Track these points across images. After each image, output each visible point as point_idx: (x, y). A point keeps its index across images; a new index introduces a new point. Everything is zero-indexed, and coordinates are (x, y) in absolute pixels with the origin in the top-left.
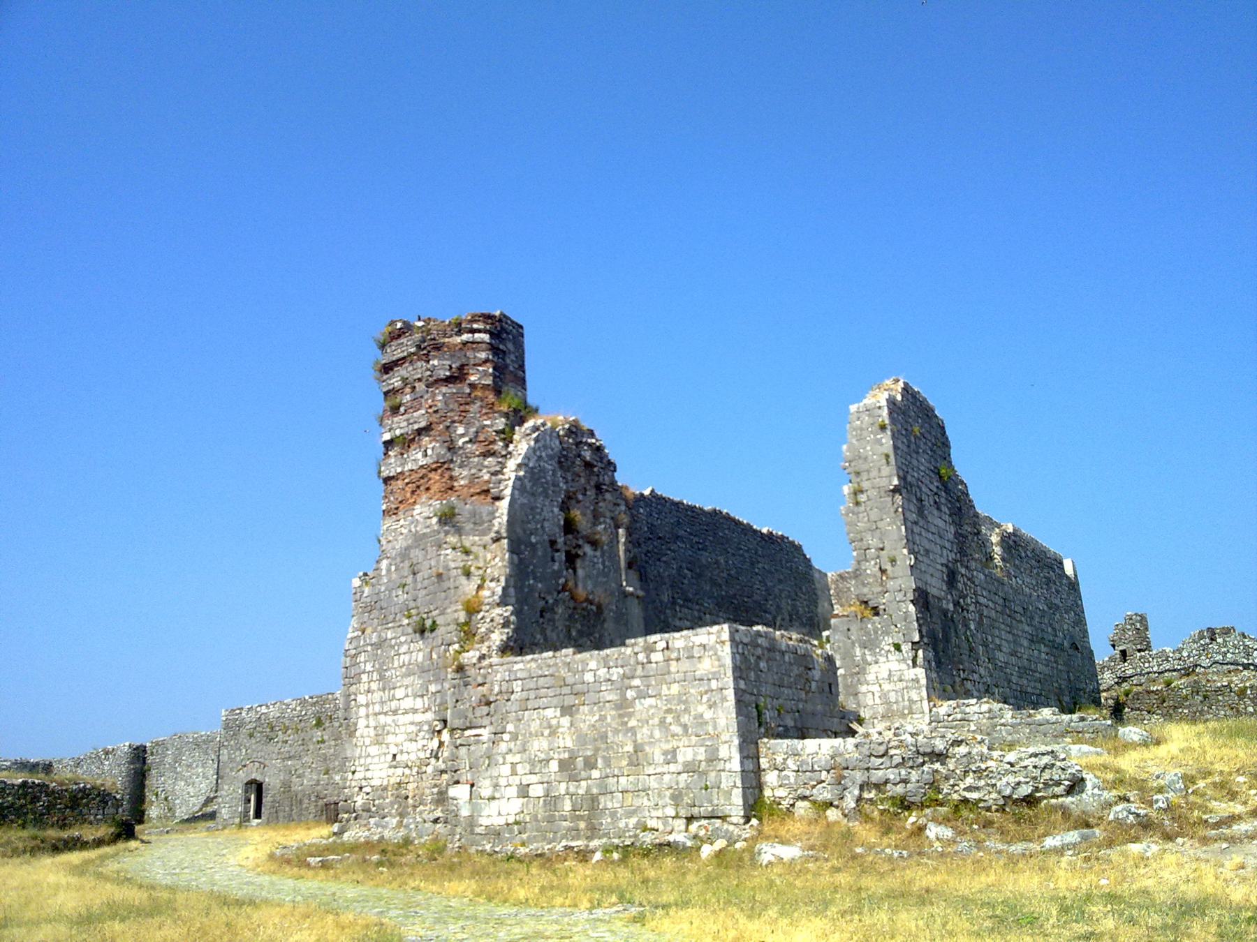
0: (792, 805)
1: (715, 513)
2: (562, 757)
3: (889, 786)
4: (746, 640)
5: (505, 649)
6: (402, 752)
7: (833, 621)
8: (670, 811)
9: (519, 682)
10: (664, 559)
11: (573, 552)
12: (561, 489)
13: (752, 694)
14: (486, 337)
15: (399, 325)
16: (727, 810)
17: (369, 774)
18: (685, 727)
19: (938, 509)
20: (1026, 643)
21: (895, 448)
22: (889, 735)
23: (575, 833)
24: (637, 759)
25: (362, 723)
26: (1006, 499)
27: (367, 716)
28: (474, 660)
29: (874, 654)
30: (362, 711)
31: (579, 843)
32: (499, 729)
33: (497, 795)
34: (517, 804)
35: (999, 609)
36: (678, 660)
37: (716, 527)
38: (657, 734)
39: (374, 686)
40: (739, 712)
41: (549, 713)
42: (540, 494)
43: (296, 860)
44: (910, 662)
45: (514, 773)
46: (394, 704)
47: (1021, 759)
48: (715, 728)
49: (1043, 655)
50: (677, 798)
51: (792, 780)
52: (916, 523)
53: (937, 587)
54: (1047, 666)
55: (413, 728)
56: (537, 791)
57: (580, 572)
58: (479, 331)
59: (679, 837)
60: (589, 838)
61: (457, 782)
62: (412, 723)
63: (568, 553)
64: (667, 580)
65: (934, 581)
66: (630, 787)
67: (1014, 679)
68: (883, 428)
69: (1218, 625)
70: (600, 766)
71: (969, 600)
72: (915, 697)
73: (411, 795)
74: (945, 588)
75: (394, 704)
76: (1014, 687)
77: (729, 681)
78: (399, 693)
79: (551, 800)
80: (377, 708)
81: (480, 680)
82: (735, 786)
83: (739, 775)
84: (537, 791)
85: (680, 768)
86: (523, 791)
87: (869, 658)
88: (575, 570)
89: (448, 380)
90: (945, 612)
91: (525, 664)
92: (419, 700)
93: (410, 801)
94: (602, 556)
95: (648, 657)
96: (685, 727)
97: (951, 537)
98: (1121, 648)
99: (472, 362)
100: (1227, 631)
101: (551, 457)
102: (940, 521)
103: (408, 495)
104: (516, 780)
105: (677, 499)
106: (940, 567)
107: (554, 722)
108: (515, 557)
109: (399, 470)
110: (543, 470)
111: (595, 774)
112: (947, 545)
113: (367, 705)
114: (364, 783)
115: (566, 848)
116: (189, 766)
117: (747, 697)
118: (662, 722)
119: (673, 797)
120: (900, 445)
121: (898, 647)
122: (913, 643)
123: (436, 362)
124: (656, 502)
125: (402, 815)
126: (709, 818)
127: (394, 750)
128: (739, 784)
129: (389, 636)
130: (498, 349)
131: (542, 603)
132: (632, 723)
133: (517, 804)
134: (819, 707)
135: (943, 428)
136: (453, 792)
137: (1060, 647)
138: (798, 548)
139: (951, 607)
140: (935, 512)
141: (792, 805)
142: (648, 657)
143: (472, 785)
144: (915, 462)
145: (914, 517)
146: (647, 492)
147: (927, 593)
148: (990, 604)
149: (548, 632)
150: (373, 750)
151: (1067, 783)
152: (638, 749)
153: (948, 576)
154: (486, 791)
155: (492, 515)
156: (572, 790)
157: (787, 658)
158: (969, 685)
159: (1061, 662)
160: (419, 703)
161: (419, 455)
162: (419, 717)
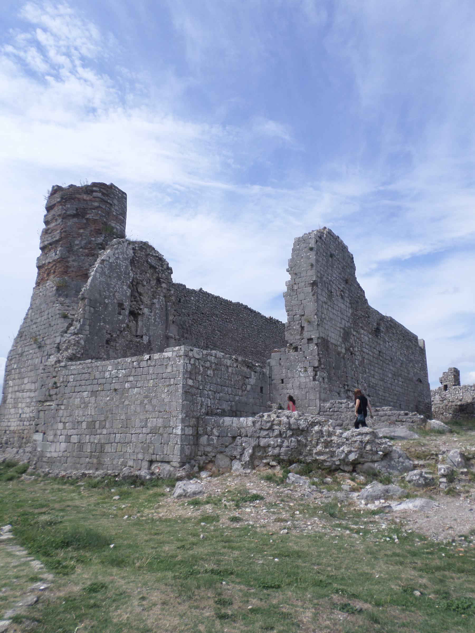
0: (215, 456)
1: (238, 305)
3: (270, 449)
9: (73, 376)
10: (204, 324)
11: (136, 311)
12: (130, 277)
13: (198, 388)
14: (99, 195)
17: (9, 424)
18: (154, 406)
20: (390, 375)
21: (317, 261)
24: (126, 426)
32: (60, 403)
33: (55, 441)
34: (63, 445)
35: (375, 356)
36: (155, 366)
41: (85, 394)
42: (115, 277)
44: (311, 378)
45: (64, 428)
48: (170, 408)
49: (400, 383)
50: (145, 450)
51: (215, 441)
53: (334, 337)
54: (402, 388)
55: (28, 400)
56: (75, 439)
57: (140, 323)
58: (96, 191)
59: (144, 473)
60: (97, 469)
64: (204, 335)
66: (122, 441)
67: (381, 393)
68: (311, 249)
70: (107, 427)
71: (356, 349)
72: (312, 397)
73: (25, 437)
74: (341, 340)
76: (380, 397)
78: (26, 381)
79: (81, 445)
81: (54, 374)
82: (177, 444)
83: (179, 437)
84: (75, 439)
86: (68, 437)
87: (289, 375)
88: (137, 322)
89: (74, 216)
90: (339, 353)
92: (33, 384)
93: (24, 440)
94: (155, 315)
95: (139, 364)
96: (154, 406)
97: (349, 315)
98: (445, 384)
99: (90, 207)
103: (45, 276)
104: (65, 432)
105: (216, 294)
106: (338, 329)
107: (87, 400)
108: (92, 309)
109: (44, 262)
111: (105, 431)
118: (142, 403)
119: (143, 448)
120: (321, 259)
122: (314, 367)
123: (69, 206)
126: (162, 462)
127: (20, 411)
128: (179, 443)
131: (109, 336)
133: (63, 445)
134: (251, 400)
135: (352, 258)
137: (411, 380)
139: (343, 351)
140: (340, 300)
141: (215, 456)
142: (139, 364)
143: (44, 433)
144: (330, 272)
147: (328, 341)
148: (370, 353)
150: (12, 411)
151: (381, 453)
152: (128, 419)
153: (344, 334)
154: (51, 438)
156: (92, 440)
157: (230, 370)
159: (410, 387)
160: (33, 387)
162: (32, 394)
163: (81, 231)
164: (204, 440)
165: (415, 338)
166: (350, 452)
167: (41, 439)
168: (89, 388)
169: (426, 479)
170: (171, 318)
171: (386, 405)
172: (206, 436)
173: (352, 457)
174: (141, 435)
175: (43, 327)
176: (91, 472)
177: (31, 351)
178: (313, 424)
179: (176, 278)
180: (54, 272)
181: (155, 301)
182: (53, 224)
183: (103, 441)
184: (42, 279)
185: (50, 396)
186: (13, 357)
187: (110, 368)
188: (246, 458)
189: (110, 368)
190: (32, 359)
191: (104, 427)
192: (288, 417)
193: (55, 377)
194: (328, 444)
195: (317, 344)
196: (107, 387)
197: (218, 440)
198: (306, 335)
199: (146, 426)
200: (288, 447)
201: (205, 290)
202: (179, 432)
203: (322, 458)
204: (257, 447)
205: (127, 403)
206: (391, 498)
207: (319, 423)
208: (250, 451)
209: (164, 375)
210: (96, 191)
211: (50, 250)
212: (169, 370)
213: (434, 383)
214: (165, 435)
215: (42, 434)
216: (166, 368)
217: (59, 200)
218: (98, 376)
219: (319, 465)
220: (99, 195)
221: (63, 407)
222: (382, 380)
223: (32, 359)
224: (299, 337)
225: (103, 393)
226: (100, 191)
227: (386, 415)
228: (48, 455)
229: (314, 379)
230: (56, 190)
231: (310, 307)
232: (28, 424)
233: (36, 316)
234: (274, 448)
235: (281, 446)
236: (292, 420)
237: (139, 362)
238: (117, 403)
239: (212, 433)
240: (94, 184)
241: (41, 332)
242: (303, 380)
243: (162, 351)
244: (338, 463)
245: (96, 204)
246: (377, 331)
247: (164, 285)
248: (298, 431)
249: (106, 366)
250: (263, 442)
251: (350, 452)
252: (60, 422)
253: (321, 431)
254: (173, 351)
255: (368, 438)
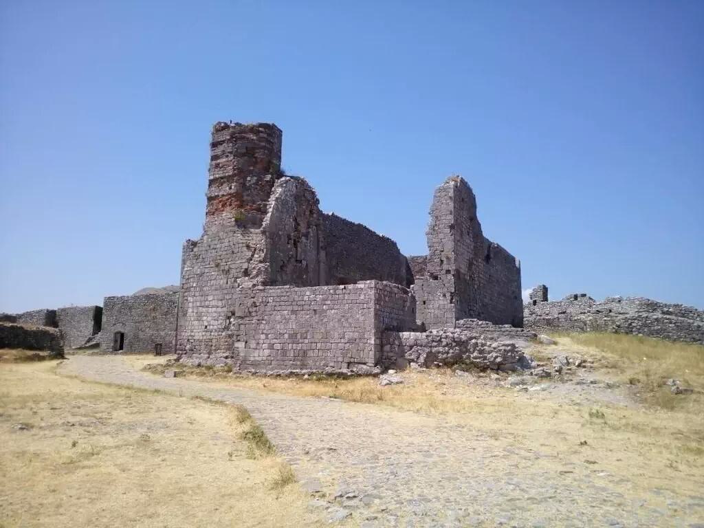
1: (359, 225)
2: (290, 332)
4: (381, 288)
5: (264, 284)
6: (210, 325)
7: (416, 281)
8: (340, 359)
14: (265, 136)
15: (222, 125)
16: (367, 360)
17: (192, 334)
18: (350, 324)
19: (468, 235)
20: (496, 295)
22: (441, 333)
23: (295, 366)
24: (326, 336)
25: (190, 310)
26: (492, 231)
27: (193, 307)
28: (250, 286)
29: (432, 295)
30: (191, 305)
31: (297, 371)
32: (261, 318)
34: (267, 352)
36: (349, 294)
37: (360, 232)
38: (337, 325)
39: (197, 294)
40: (375, 319)
41: (286, 312)
43: (151, 369)
44: (449, 301)
45: (267, 338)
46: (207, 303)
47: (499, 346)
52: (458, 241)
53: (464, 270)
56: (278, 346)
61: (239, 341)
62: (215, 312)
63: (295, 240)
65: (463, 266)
69: (579, 293)
73: (214, 345)
75: (207, 303)
77: (372, 304)
78: (210, 298)
79: (284, 352)
80: (198, 304)
81: (252, 295)
84: (278, 346)
85: (346, 341)
91: (274, 291)
92: (220, 302)
93: (213, 348)
95: (335, 292)
96: (350, 324)
100: (584, 295)
101: (291, 196)
102: (468, 240)
105: (344, 217)
109: (216, 194)
110: (287, 201)
111: (306, 341)
112: (470, 250)
113: (193, 302)
114: (190, 338)
115: (291, 372)
116: (78, 322)
117: (379, 313)
118: (339, 320)
121: (444, 296)
124: (334, 218)
125: (210, 353)
127: (206, 324)
128: (373, 349)
129: (206, 271)
130: (270, 141)
132: (325, 320)
133: (267, 352)
136: (237, 345)
138: (394, 244)
142: (335, 292)
143: (246, 342)
145: (458, 238)
146: (330, 214)
149: (283, 276)
150: (196, 323)
152: (327, 332)
155: (262, 220)
158: (472, 312)
160: (220, 304)
161: (227, 188)
162: (219, 310)
163: (252, 168)
164: (387, 348)
165: (513, 259)
166: (497, 357)
167: (244, 347)
168: (290, 308)
169: (546, 372)
170: (321, 244)
171: (507, 324)
172: (389, 346)
173: (499, 360)
174: (340, 344)
175: (225, 253)
176: (297, 371)
177: (213, 273)
178: (471, 338)
179: (326, 207)
180: (230, 205)
181: (310, 230)
182: (224, 160)
183: (305, 348)
184: (216, 210)
185: (250, 313)
186: (192, 276)
187: (308, 293)
188: (422, 360)
189: (308, 293)
190: (215, 279)
191: (306, 338)
192: (452, 333)
193: (253, 298)
194: (481, 352)
195: (453, 275)
196: (306, 307)
197: (398, 348)
198: (445, 267)
199: (344, 338)
200: (453, 353)
201: (336, 214)
202: (373, 342)
203: (478, 360)
204: (429, 354)
205: (325, 320)
206: (526, 384)
207: (475, 338)
208: (425, 356)
209: (358, 301)
210: (262, 132)
211: (222, 185)
212: (362, 297)
213: (526, 295)
214: (361, 344)
215: (244, 343)
216: (360, 296)
217: (228, 137)
218: (296, 298)
219: (476, 365)
220: (265, 136)
221: (264, 322)
222: (491, 300)
223: (215, 279)
224: (439, 268)
225: (302, 312)
226: (265, 133)
227: (507, 331)
228: (252, 359)
229: (451, 303)
230: (221, 128)
231: (449, 245)
232: (216, 334)
233: (214, 242)
234: (443, 354)
235: (448, 353)
236: (456, 335)
237: (335, 290)
238: (317, 320)
239: (394, 343)
240: (261, 125)
241: (222, 257)
242: (441, 302)
243: (356, 283)
244: (488, 364)
245: (263, 144)
246: (488, 258)
247: (315, 215)
248: (460, 343)
249: (305, 292)
250: (434, 350)
251: (497, 357)
252: (263, 333)
253: (477, 343)
254: (365, 283)
255: (509, 348)
